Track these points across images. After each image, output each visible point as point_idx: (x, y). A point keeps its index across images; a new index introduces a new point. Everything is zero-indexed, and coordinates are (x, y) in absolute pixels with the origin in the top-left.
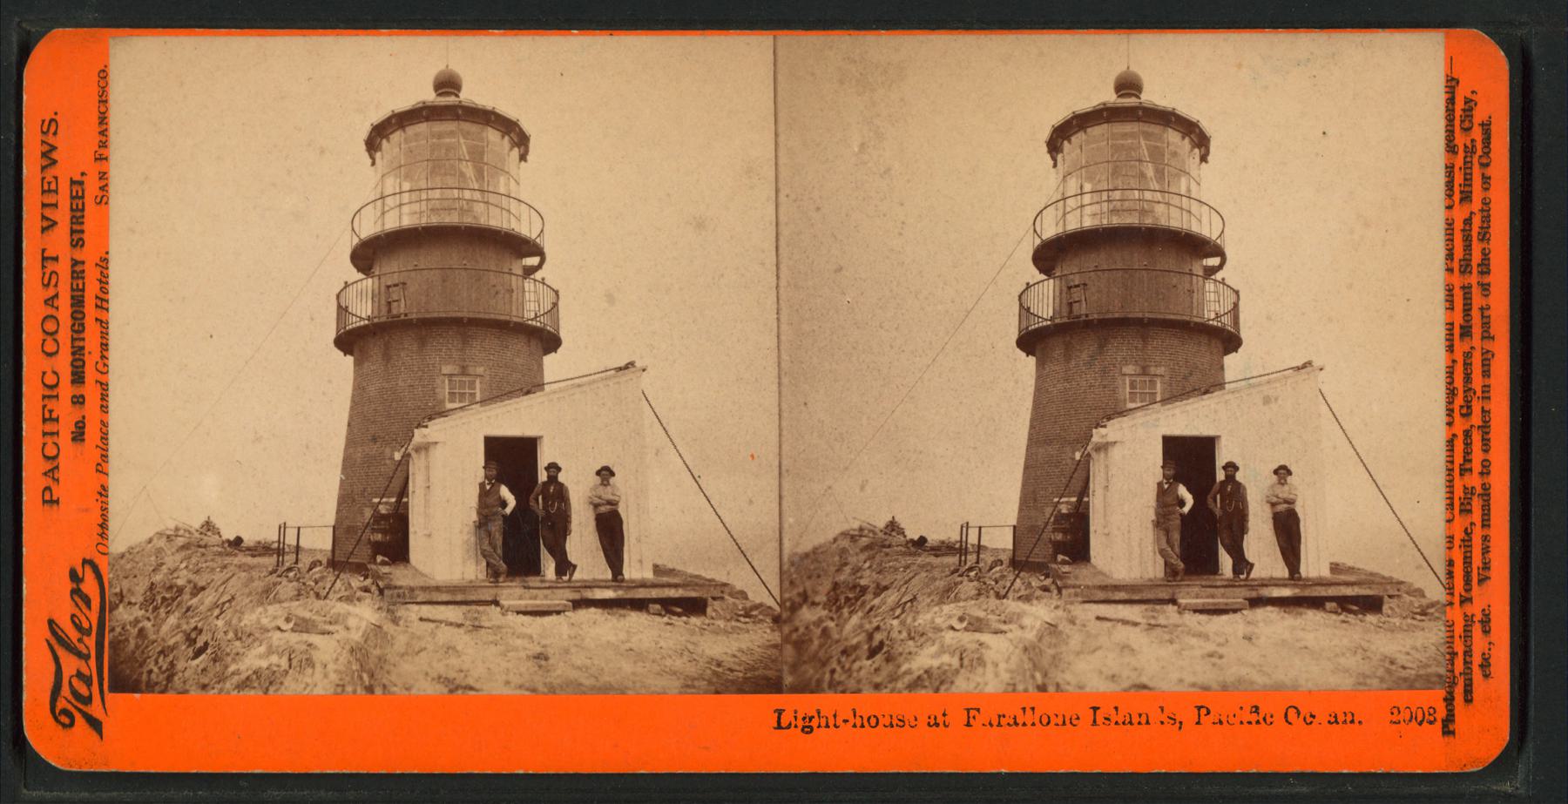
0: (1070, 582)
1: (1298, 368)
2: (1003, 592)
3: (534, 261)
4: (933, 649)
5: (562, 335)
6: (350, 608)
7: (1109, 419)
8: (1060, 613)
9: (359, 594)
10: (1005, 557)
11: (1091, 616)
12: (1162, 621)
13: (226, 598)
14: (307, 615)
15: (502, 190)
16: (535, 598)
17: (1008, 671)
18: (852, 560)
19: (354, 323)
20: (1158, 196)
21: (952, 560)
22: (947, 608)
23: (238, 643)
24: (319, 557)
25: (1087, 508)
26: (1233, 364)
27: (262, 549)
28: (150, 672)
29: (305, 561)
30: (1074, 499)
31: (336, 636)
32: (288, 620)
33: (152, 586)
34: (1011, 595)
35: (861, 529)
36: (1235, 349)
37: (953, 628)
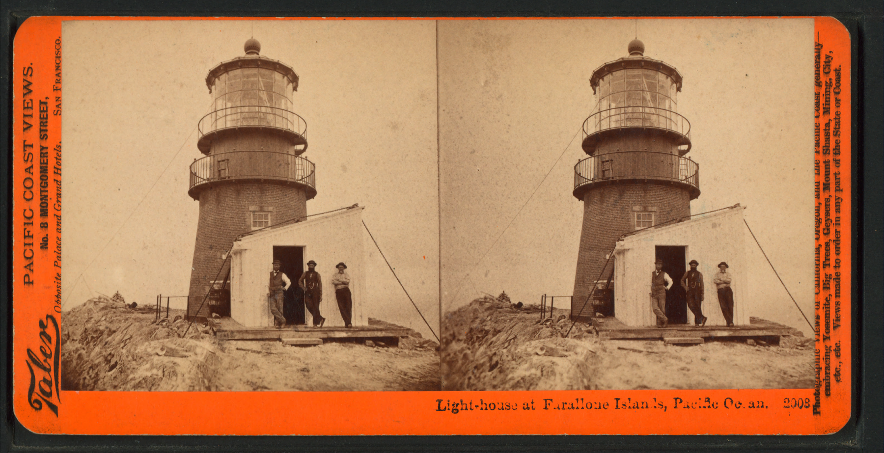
1: (350, 208)
2: (565, 334)
3: (301, 147)
4: (526, 366)
10: (567, 314)
11: (615, 347)
12: (655, 350)
14: (173, 346)
15: (283, 107)
18: (481, 315)
19: (199, 182)
20: (653, 111)
21: (537, 316)
22: (534, 343)
24: (180, 314)
25: (613, 286)
26: (695, 205)
27: (148, 309)
28: (85, 378)
29: (172, 316)
30: (605, 281)
31: (190, 358)
32: (162, 349)
33: (86, 330)
34: (570, 335)
35: (485, 298)
36: (696, 197)
37: (537, 354)
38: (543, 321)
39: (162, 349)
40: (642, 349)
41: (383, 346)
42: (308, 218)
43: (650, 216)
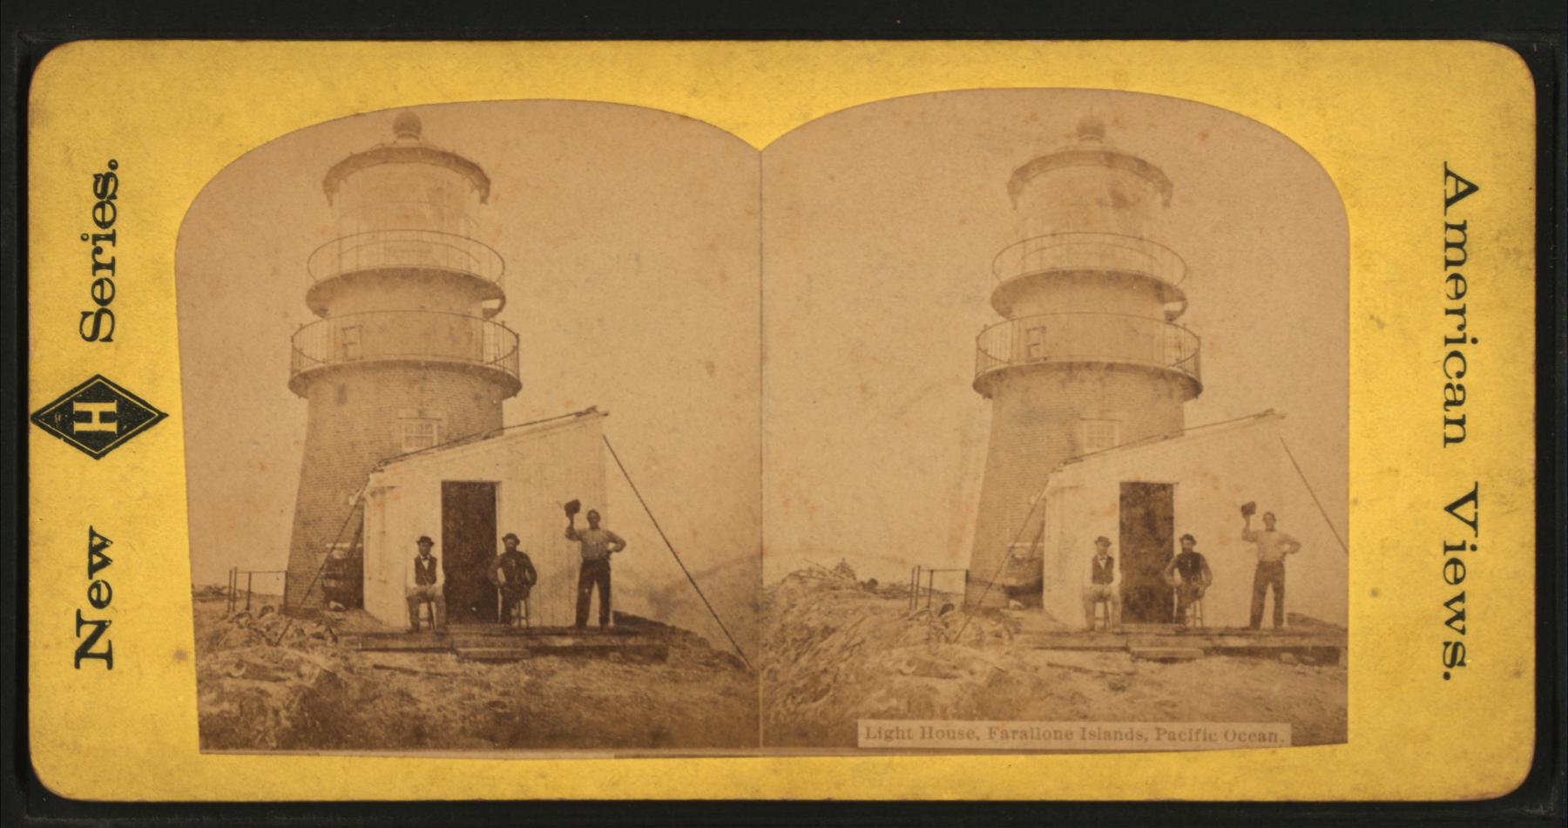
2: (275, 639)
3: (495, 304)
4: (882, 693)
5: (523, 379)
7: (387, 463)
8: (1010, 659)
9: (312, 641)
10: (275, 604)
11: (1042, 663)
12: (442, 670)
13: (857, 640)
14: (259, 662)
15: (463, 233)
16: (493, 645)
17: (288, 718)
18: (801, 602)
19: (307, 366)
21: (903, 604)
22: (895, 653)
23: (858, 687)
24: (270, 603)
26: (513, 410)
27: (893, 592)
28: (778, 713)
29: (257, 606)
30: (1028, 544)
31: (289, 684)
32: (909, 664)
33: (784, 628)
34: (283, 642)
35: (810, 570)
37: (901, 673)
40: (1088, 666)
42: (1188, 433)
43: (430, 425)
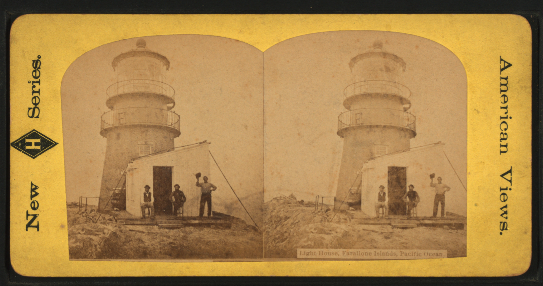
0: (119, 217)
1: (436, 144)
2: (95, 221)
3: (171, 105)
4: (305, 239)
6: (338, 225)
7: (134, 160)
10: (95, 209)
11: (361, 229)
12: (153, 231)
13: (297, 221)
14: (90, 228)
15: (160, 80)
16: (171, 223)
17: (100, 248)
18: (277, 208)
19: (106, 127)
20: (151, 82)
21: (313, 209)
22: (310, 225)
23: (297, 237)
24: (94, 208)
25: (361, 191)
26: (178, 142)
27: (309, 205)
29: (89, 209)
30: (356, 188)
31: (100, 236)
32: (315, 229)
33: (271, 217)
34: (98, 222)
35: (281, 197)
36: (178, 136)
37: (312, 232)
38: (316, 212)
39: (315, 229)
41: (454, 229)
42: (411, 150)
